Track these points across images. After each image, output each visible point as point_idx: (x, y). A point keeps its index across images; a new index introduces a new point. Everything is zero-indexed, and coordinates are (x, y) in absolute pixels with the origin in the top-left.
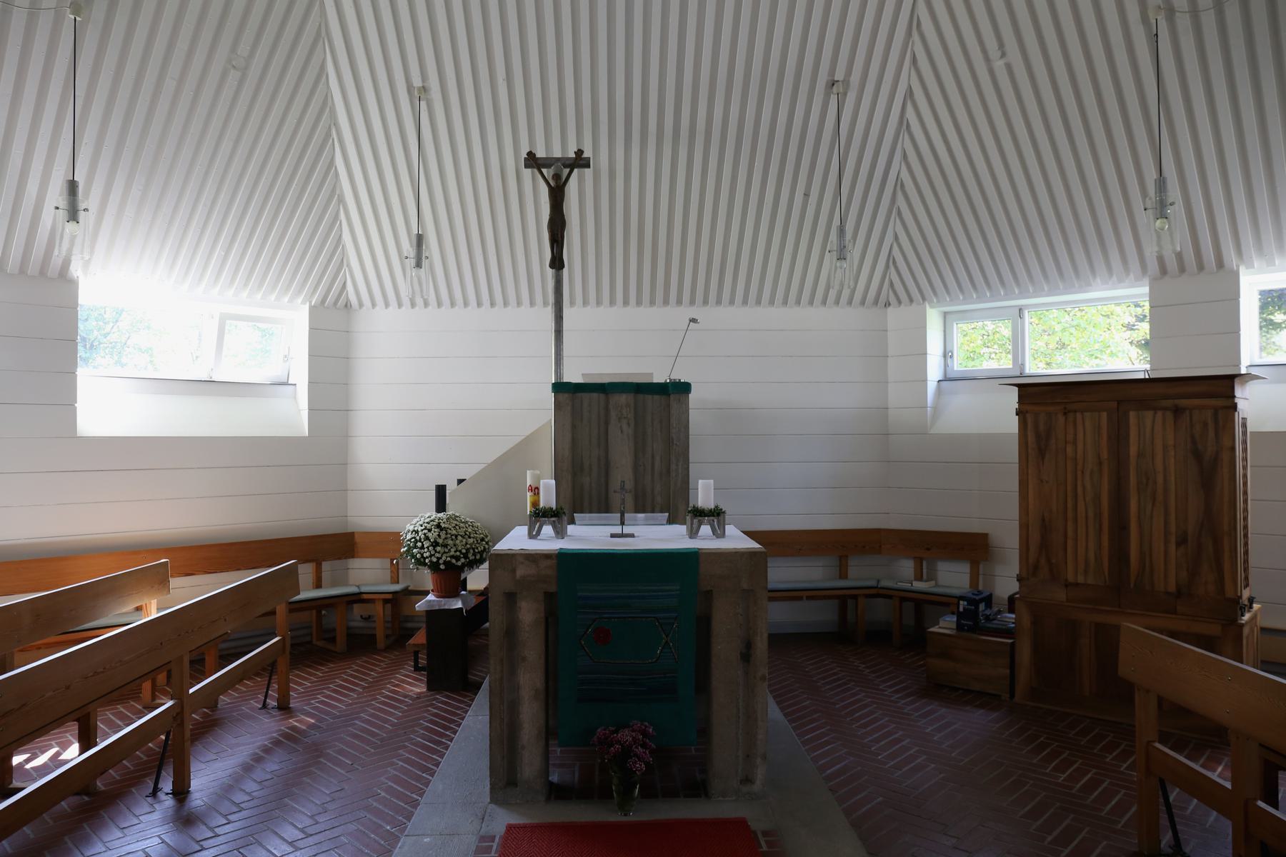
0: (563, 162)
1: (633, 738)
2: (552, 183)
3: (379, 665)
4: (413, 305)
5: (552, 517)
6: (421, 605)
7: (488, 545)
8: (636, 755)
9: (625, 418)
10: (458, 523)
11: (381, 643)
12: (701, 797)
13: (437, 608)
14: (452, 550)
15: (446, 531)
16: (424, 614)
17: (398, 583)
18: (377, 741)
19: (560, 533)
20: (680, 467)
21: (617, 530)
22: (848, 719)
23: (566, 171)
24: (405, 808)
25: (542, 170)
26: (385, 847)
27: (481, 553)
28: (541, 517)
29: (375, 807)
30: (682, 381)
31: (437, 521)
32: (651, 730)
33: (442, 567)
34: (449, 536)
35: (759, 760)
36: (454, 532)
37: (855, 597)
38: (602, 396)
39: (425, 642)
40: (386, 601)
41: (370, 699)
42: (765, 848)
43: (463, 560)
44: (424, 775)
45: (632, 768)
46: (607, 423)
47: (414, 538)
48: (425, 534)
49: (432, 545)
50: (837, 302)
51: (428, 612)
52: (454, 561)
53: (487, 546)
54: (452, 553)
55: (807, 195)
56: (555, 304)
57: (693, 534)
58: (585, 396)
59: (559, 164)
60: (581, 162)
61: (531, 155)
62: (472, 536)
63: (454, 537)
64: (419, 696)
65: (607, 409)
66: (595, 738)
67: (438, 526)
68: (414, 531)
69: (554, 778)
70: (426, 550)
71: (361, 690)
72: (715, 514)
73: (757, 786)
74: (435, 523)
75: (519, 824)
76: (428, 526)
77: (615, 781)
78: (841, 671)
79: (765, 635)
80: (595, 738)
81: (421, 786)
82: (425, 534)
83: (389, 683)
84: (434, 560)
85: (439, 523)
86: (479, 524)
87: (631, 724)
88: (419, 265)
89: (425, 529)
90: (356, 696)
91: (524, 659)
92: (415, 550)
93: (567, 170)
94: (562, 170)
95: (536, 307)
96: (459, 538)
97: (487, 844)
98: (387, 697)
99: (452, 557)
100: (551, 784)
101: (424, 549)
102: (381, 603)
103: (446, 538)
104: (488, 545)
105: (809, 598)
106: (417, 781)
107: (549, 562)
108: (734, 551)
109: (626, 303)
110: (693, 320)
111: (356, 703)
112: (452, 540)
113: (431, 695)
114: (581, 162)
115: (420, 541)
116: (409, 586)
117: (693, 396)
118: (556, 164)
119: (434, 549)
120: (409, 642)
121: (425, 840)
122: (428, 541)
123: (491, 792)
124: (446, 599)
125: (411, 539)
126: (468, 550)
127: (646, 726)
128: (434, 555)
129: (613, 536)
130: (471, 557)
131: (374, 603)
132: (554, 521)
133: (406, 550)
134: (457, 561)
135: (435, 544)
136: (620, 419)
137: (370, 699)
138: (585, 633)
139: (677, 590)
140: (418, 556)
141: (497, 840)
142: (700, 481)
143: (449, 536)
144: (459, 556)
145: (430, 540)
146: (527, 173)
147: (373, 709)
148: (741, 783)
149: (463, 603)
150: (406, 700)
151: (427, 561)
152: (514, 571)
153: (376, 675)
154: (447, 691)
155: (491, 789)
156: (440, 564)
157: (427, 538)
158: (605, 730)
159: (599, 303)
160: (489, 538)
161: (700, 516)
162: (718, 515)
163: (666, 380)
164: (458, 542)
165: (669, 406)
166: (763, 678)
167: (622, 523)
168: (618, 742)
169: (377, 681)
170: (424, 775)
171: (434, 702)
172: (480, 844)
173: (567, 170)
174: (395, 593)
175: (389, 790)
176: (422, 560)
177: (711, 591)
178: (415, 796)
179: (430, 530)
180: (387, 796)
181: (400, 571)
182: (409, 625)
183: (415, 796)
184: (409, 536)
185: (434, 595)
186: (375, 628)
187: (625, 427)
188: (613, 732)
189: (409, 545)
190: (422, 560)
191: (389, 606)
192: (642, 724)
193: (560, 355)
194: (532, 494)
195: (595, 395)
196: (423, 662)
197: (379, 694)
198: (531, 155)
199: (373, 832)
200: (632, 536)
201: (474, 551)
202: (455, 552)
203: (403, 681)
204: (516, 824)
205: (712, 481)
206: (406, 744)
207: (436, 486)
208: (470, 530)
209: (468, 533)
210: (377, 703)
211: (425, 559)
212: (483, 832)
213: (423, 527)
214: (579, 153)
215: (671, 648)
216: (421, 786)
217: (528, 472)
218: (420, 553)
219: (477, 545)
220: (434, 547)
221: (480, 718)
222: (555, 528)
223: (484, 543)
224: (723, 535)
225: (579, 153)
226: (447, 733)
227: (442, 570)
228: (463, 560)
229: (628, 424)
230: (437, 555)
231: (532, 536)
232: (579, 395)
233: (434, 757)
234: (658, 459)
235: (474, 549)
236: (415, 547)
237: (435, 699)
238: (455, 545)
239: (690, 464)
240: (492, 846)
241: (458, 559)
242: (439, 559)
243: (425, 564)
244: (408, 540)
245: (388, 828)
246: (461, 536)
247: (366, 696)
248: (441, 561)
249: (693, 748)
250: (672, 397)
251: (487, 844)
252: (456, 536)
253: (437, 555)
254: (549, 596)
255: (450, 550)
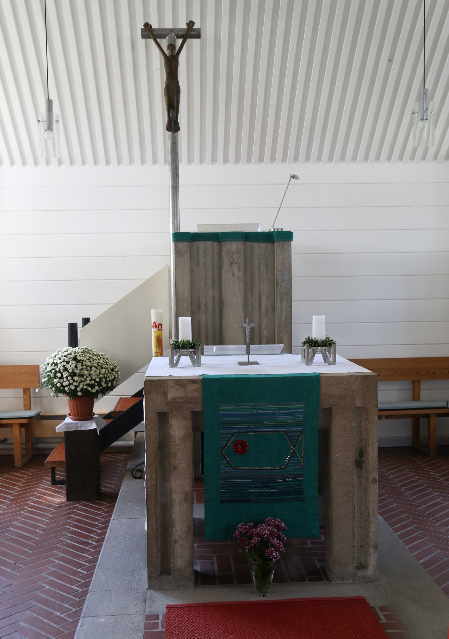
0: (176, 33)
1: (270, 531)
2: (167, 52)
3: (20, 481)
4: (48, 163)
5: (190, 348)
6: (60, 427)
7: (117, 374)
8: (273, 546)
9: (236, 263)
10: (91, 356)
11: (18, 461)
12: (323, 581)
13: (74, 429)
14: (88, 379)
15: (82, 363)
16: (63, 435)
17: (30, 409)
18: (33, 544)
19: (196, 363)
20: (284, 304)
21: (244, 359)
22: (431, 519)
23: (180, 41)
24: (68, 598)
25: (158, 40)
26: (59, 629)
27: (112, 381)
28: (181, 349)
29: (43, 597)
30: (284, 230)
31: (73, 354)
32: (283, 525)
33: (79, 394)
34: (84, 367)
35: (371, 550)
36: (89, 364)
37: (427, 416)
38: (216, 244)
39: (64, 459)
40: (22, 425)
41: (18, 509)
42: (384, 620)
43: (97, 388)
44: (79, 570)
45: (269, 556)
46: (220, 268)
47: (54, 369)
48: (64, 366)
49: (70, 375)
50: (424, 158)
51: (66, 433)
52: (89, 389)
53: (116, 376)
54: (88, 382)
55: (390, 60)
56: (172, 163)
57: (309, 361)
58: (201, 244)
59: (173, 35)
60: (192, 33)
61: (147, 25)
62: (104, 366)
63: (88, 368)
64: (61, 506)
65: (220, 256)
66: (237, 532)
67: (75, 359)
68: (53, 363)
69: (198, 568)
70: (65, 380)
71: (9, 502)
72: (328, 344)
73: (370, 571)
74: (72, 356)
75: (177, 605)
76: (66, 359)
77: (254, 567)
78: (418, 479)
79: (376, 445)
80: (237, 532)
81: (79, 579)
82: (64, 366)
83: (33, 495)
84: (73, 388)
85: (76, 356)
86: (108, 356)
87: (266, 520)
88: (50, 128)
89: (64, 361)
90: (5, 507)
91: (175, 468)
92: (55, 380)
93: (180, 41)
94: (175, 41)
95: (146, 165)
96: (93, 368)
97: (153, 621)
98: (32, 507)
99: (88, 385)
100: (196, 572)
101: (63, 379)
102: (18, 427)
103: (82, 369)
104: (117, 374)
105: (387, 417)
106: (74, 575)
107: (195, 386)
108: (350, 375)
109: (226, 160)
110: (293, 177)
111: (7, 513)
112: (87, 370)
113: (71, 505)
114: (192, 33)
115: (59, 372)
116: (41, 412)
117: (294, 243)
118: (170, 35)
119: (72, 379)
120: (47, 460)
121: (101, 620)
122: (66, 372)
123: (149, 580)
124: (82, 422)
125: (51, 371)
126: (101, 379)
127: (279, 522)
128: (72, 384)
129: (241, 364)
130: (104, 385)
131: (12, 427)
132: (191, 352)
133: (47, 380)
134: (92, 389)
135: (73, 374)
136: (231, 264)
137: (18, 509)
138: (226, 444)
139: (302, 408)
140: (59, 385)
141: (161, 617)
142: (314, 317)
143: (84, 367)
144: (94, 384)
145: (68, 371)
146: (141, 42)
147: (23, 517)
148: (356, 569)
149: (97, 425)
150: (50, 509)
151: (66, 389)
152: (166, 394)
153: (19, 489)
154: (84, 501)
155: (149, 577)
156: (78, 391)
157: (66, 369)
158: (244, 525)
159: (202, 161)
160: (118, 368)
161: (315, 346)
162: (330, 345)
163: (270, 229)
164: (92, 372)
165: (273, 252)
166: (374, 481)
167: (248, 353)
168: (258, 535)
169: (21, 494)
170: (79, 570)
171: (75, 510)
172: (147, 622)
173: (180, 41)
174: (30, 418)
175: (52, 584)
176: (62, 388)
177: (331, 408)
178: (75, 588)
179: (68, 363)
180: (51, 589)
181: (32, 399)
182: (41, 446)
183: (75, 588)
184: (49, 368)
185: (71, 418)
186: (13, 449)
187: (236, 271)
188: (252, 527)
189: (49, 375)
190: (62, 388)
191: (23, 429)
192: (275, 520)
193: (177, 208)
194: (156, 329)
195: (209, 244)
196: (60, 475)
197: (26, 505)
198: (147, 25)
199: (46, 618)
200: (256, 363)
201: (106, 379)
202: (90, 380)
203: (44, 494)
204: (174, 605)
205: (324, 316)
206: (58, 545)
207: (68, 324)
208: (102, 362)
209: (100, 364)
210: (26, 512)
211: (64, 387)
212: (148, 612)
213: (62, 360)
214: (191, 24)
215: (297, 457)
216: (79, 579)
217: (152, 310)
218: (59, 382)
219: (109, 375)
220: (72, 377)
221: (124, 521)
222: (192, 358)
223: (114, 372)
224: (334, 362)
225: (191, 24)
226: (92, 535)
227: (79, 396)
228: (97, 388)
229: (239, 268)
230: (75, 384)
231: (173, 364)
232: (196, 243)
233: (84, 555)
234: (264, 298)
235: (106, 378)
236: (55, 377)
237: (76, 508)
238: (90, 375)
239: (292, 302)
240: (158, 623)
241: (92, 386)
242: (76, 387)
243: (64, 392)
244: (48, 372)
245: (58, 614)
246: (95, 367)
247: (14, 507)
248: (78, 389)
249: (309, 541)
250: (276, 244)
251: (153, 621)
252: (91, 367)
253: (75, 384)
254: (195, 414)
255: (86, 379)
